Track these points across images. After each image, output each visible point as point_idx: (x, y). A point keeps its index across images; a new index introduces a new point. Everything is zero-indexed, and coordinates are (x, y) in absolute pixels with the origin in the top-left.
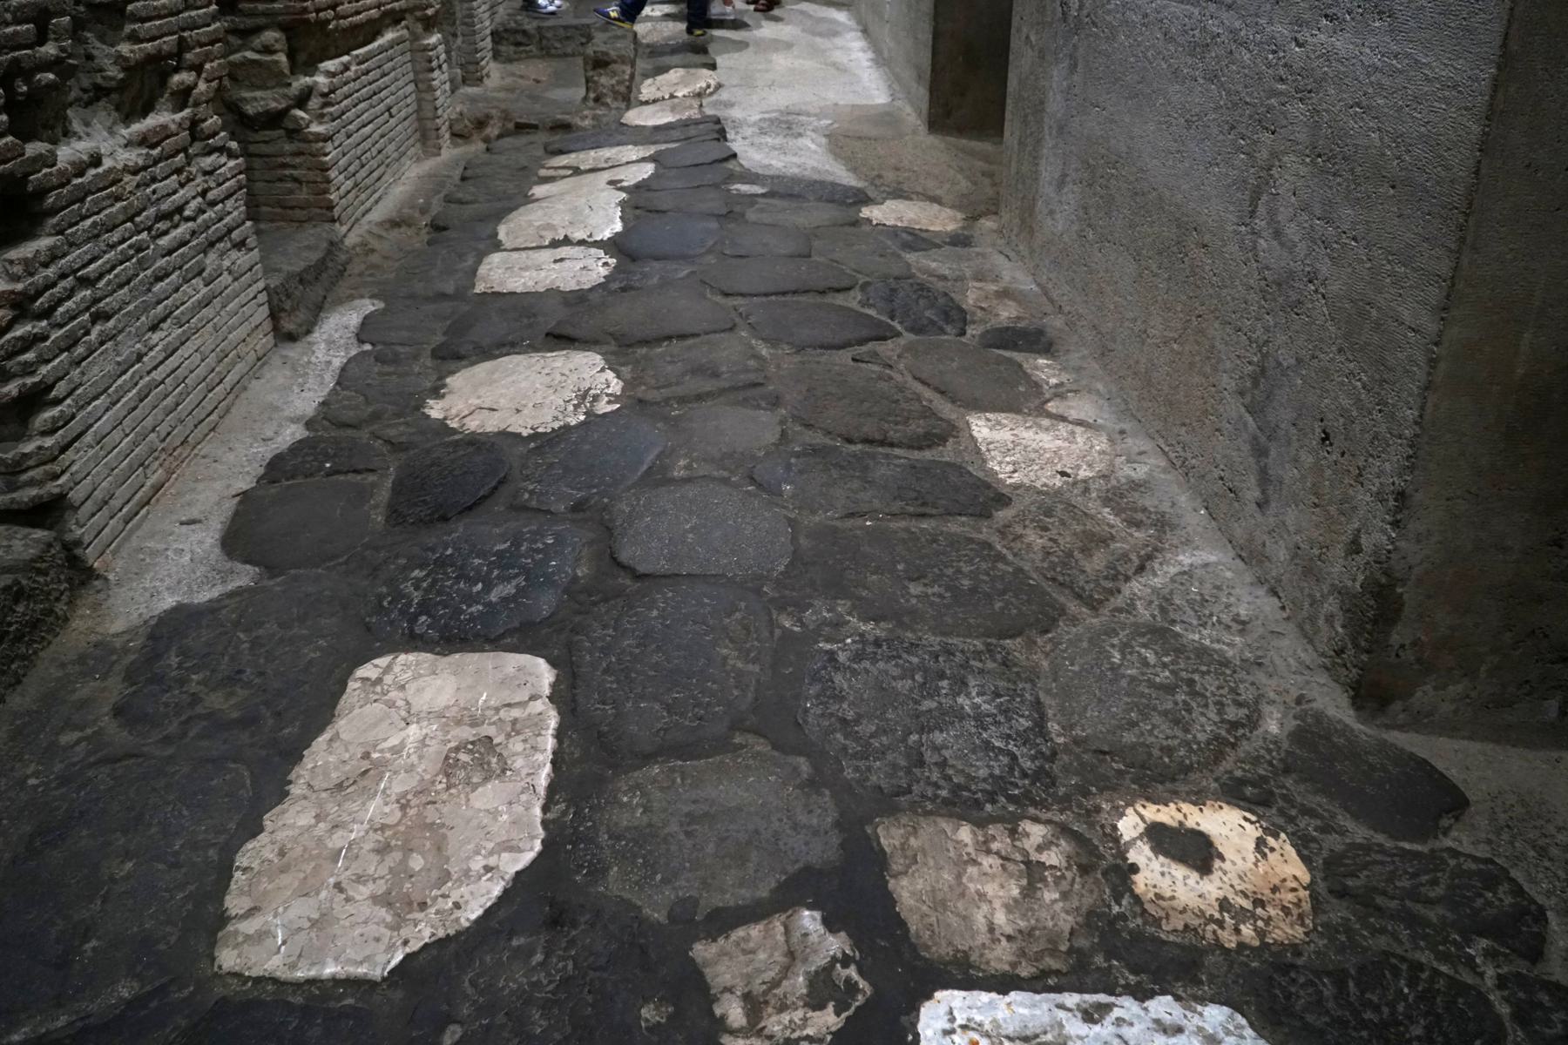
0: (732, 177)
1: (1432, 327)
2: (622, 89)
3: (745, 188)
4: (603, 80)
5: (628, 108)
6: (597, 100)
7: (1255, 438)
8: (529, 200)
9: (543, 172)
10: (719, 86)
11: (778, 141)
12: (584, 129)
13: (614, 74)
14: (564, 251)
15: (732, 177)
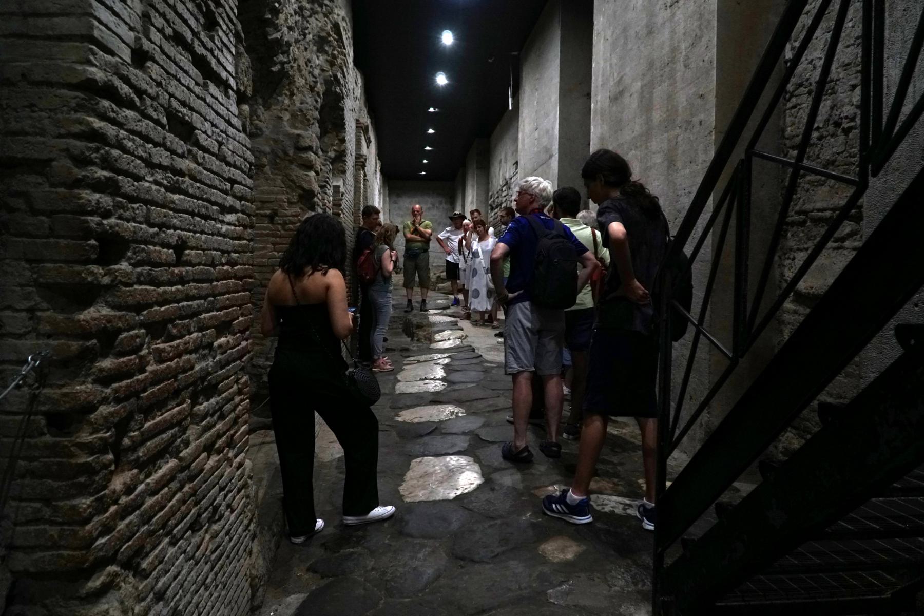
0: (482, 362)
1: (708, 357)
2: (428, 336)
3: (489, 365)
4: (420, 333)
5: (431, 343)
6: (418, 340)
7: (638, 592)
8: (403, 370)
9: (405, 362)
10: (466, 336)
11: (496, 353)
12: (414, 351)
13: (425, 330)
14: (427, 381)
15: (482, 362)
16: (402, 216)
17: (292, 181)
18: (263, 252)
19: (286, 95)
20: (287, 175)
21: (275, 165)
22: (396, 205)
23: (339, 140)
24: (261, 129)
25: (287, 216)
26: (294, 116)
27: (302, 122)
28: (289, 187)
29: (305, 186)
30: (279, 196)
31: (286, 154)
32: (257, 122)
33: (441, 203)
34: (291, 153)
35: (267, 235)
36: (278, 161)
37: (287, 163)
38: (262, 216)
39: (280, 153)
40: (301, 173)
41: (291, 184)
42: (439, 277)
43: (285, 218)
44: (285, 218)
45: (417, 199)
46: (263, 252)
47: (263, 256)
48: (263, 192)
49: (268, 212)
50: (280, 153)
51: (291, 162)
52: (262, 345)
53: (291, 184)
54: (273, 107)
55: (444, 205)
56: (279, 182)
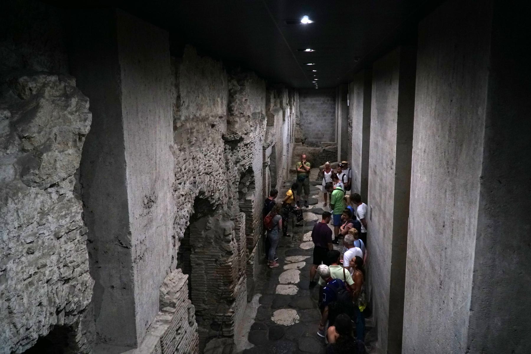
2: (300, 238)
6: (295, 240)
16: (307, 108)
17: (223, 248)
18: (213, 274)
19: (220, 209)
20: (221, 246)
21: (216, 242)
22: (303, 103)
23: (251, 177)
24: (210, 227)
25: (221, 261)
26: (224, 216)
27: (227, 218)
28: (222, 250)
29: (228, 250)
30: (218, 254)
31: (220, 237)
32: (209, 225)
33: (328, 100)
34: (222, 237)
35: (215, 268)
36: (217, 240)
37: (221, 241)
38: (212, 261)
39: (218, 237)
40: (226, 244)
41: (222, 249)
42: (324, 150)
43: (221, 262)
44: (221, 262)
45: (315, 99)
46: (213, 274)
47: (213, 276)
48: (212, 252)
49: (214, 260)
50: (218, 237)
51: (222, 241)
52: (214, 306)
53: (222, 249)
54: (215, 215)
55: (330, 102)
56: (218, 248)
